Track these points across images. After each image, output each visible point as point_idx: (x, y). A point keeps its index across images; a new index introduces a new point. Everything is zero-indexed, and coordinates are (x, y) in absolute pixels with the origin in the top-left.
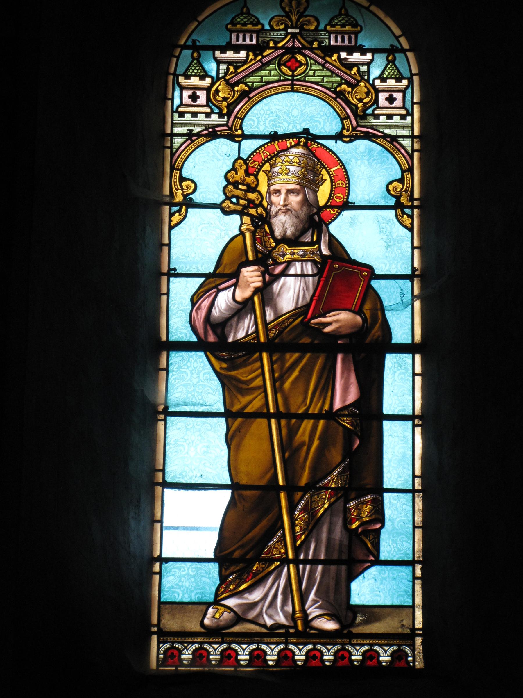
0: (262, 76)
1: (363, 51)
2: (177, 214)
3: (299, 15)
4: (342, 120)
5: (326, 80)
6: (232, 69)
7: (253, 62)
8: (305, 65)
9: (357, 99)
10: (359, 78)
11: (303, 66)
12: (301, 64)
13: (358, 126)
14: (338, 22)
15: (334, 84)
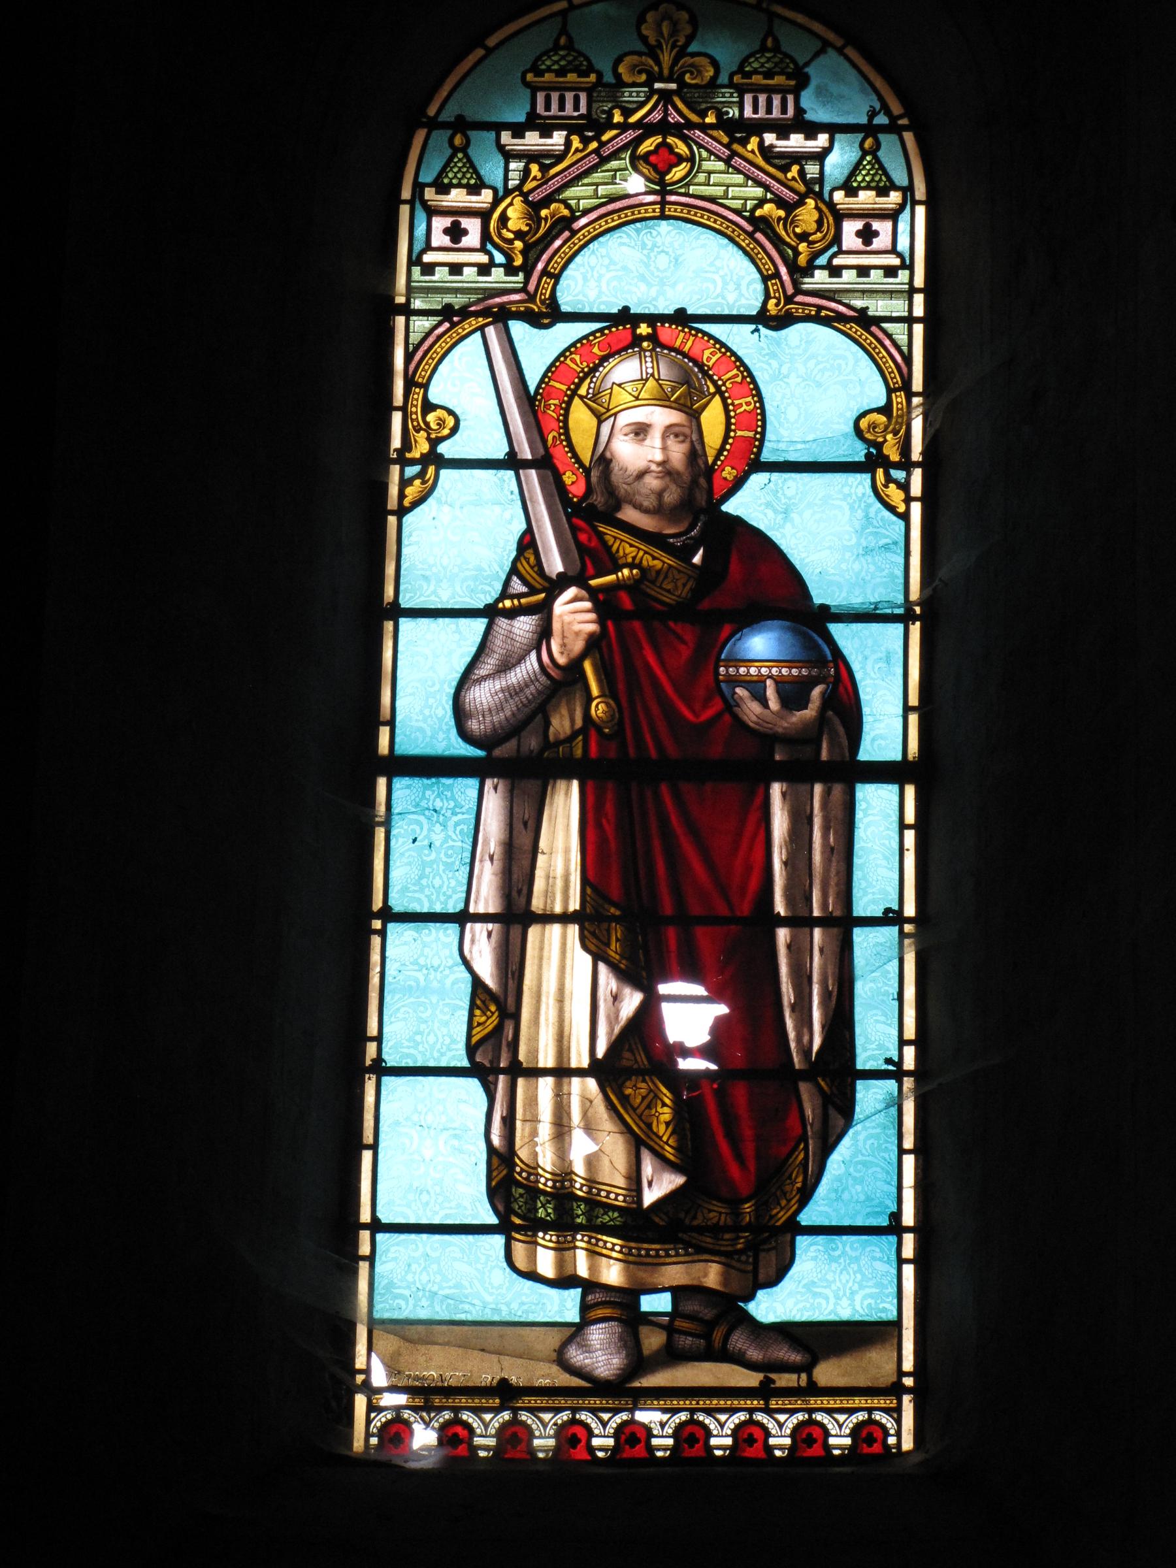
0: (597, 185)
1: (811, 130)
2: (417, 482)
3: (678, 52)
4: (765, 279)
5: (732, 192)
6: (535, 169)
7: (579, 155)
8: (687, 160)
9: (795, 234)
10: (802, 188)
11: (685, 164)
12: (680, 159)
13: (799, 291)
14: (553, 65)
15: (749, 202)
